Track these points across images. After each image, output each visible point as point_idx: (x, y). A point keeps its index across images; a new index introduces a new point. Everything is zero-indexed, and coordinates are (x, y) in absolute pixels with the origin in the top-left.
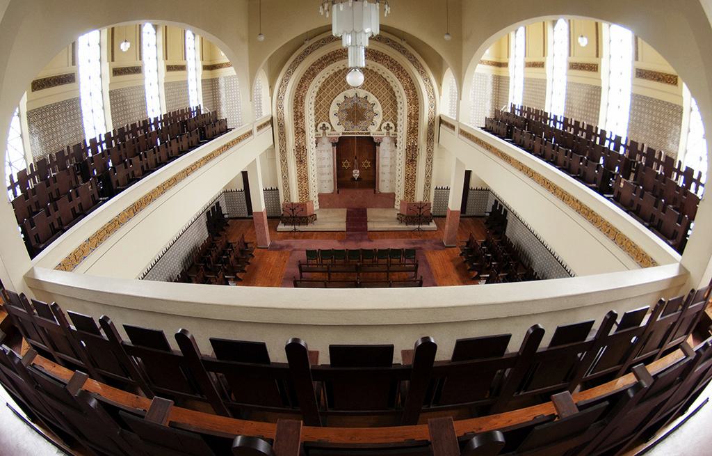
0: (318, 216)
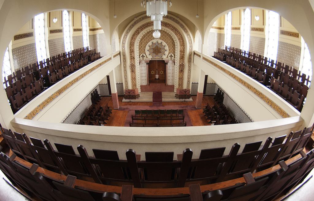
0: (140, 95)
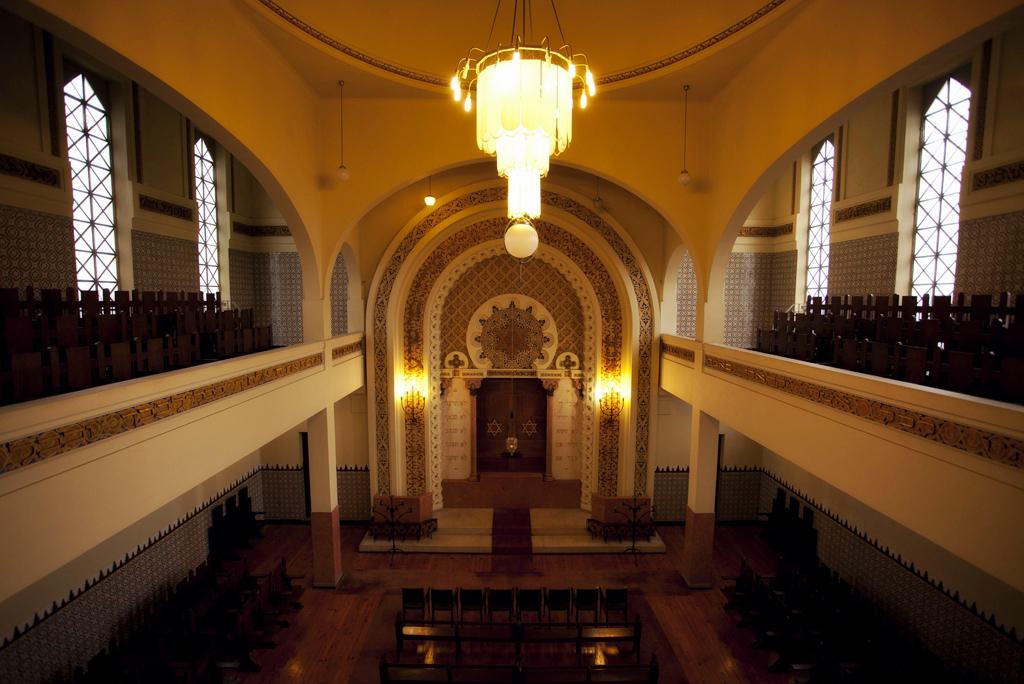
0: (440, 524)
